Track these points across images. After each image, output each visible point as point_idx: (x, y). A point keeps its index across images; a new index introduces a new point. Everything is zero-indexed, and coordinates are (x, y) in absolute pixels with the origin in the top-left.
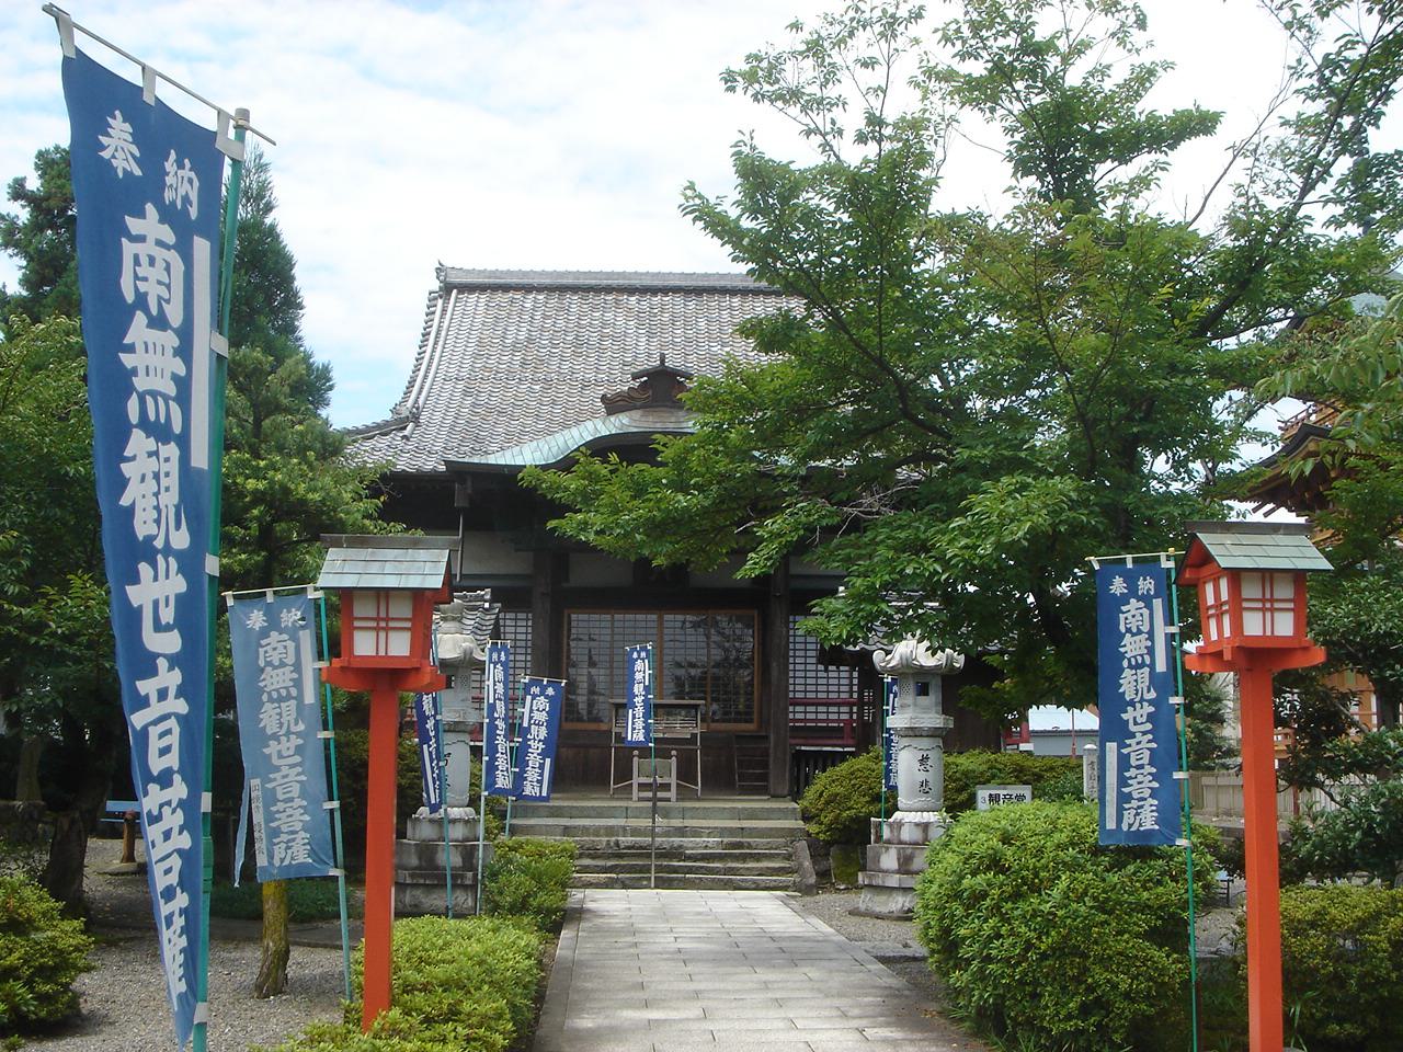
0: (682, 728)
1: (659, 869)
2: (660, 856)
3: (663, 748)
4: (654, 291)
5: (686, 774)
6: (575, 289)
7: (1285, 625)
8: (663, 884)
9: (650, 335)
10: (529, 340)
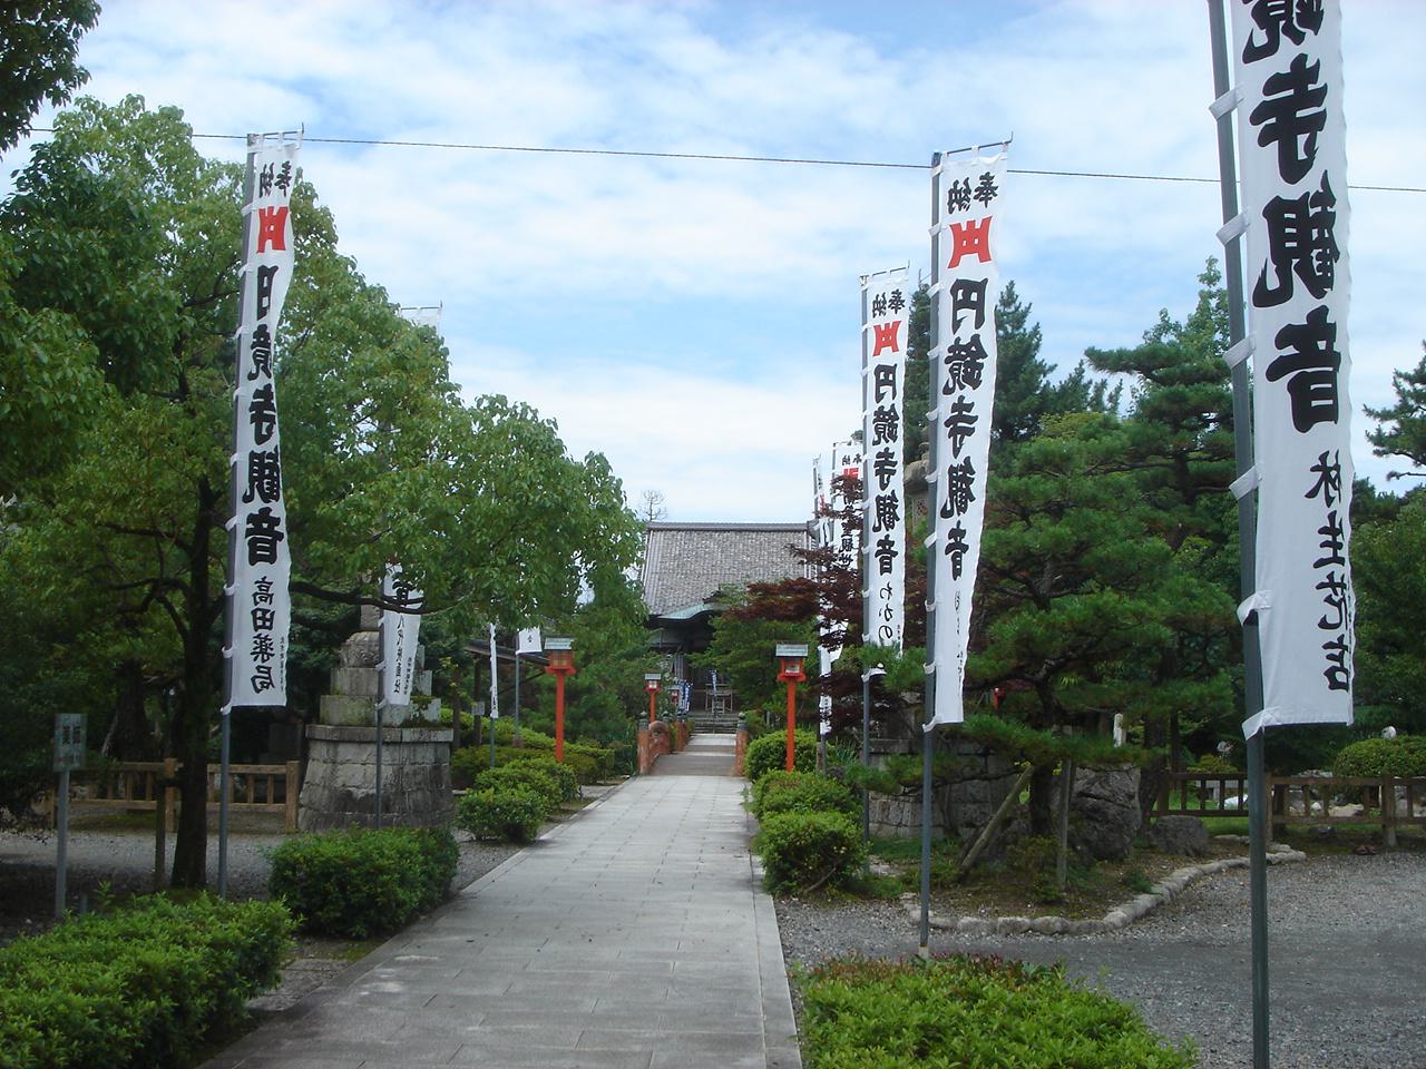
0: (727, 693)
3: (720, 699)
4: (725, 531)
5: (728, 705)
6: (791, 531)
7: (655, 687)
9: (722, 552)
10: (680, 555)
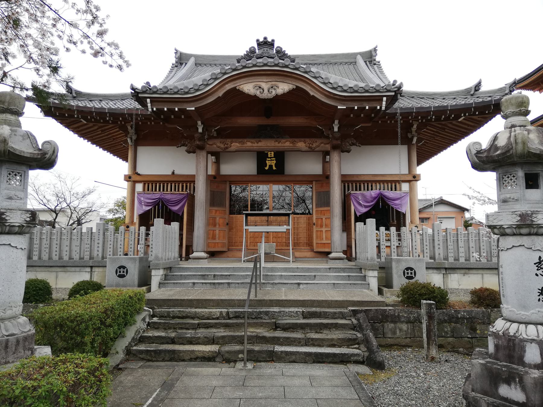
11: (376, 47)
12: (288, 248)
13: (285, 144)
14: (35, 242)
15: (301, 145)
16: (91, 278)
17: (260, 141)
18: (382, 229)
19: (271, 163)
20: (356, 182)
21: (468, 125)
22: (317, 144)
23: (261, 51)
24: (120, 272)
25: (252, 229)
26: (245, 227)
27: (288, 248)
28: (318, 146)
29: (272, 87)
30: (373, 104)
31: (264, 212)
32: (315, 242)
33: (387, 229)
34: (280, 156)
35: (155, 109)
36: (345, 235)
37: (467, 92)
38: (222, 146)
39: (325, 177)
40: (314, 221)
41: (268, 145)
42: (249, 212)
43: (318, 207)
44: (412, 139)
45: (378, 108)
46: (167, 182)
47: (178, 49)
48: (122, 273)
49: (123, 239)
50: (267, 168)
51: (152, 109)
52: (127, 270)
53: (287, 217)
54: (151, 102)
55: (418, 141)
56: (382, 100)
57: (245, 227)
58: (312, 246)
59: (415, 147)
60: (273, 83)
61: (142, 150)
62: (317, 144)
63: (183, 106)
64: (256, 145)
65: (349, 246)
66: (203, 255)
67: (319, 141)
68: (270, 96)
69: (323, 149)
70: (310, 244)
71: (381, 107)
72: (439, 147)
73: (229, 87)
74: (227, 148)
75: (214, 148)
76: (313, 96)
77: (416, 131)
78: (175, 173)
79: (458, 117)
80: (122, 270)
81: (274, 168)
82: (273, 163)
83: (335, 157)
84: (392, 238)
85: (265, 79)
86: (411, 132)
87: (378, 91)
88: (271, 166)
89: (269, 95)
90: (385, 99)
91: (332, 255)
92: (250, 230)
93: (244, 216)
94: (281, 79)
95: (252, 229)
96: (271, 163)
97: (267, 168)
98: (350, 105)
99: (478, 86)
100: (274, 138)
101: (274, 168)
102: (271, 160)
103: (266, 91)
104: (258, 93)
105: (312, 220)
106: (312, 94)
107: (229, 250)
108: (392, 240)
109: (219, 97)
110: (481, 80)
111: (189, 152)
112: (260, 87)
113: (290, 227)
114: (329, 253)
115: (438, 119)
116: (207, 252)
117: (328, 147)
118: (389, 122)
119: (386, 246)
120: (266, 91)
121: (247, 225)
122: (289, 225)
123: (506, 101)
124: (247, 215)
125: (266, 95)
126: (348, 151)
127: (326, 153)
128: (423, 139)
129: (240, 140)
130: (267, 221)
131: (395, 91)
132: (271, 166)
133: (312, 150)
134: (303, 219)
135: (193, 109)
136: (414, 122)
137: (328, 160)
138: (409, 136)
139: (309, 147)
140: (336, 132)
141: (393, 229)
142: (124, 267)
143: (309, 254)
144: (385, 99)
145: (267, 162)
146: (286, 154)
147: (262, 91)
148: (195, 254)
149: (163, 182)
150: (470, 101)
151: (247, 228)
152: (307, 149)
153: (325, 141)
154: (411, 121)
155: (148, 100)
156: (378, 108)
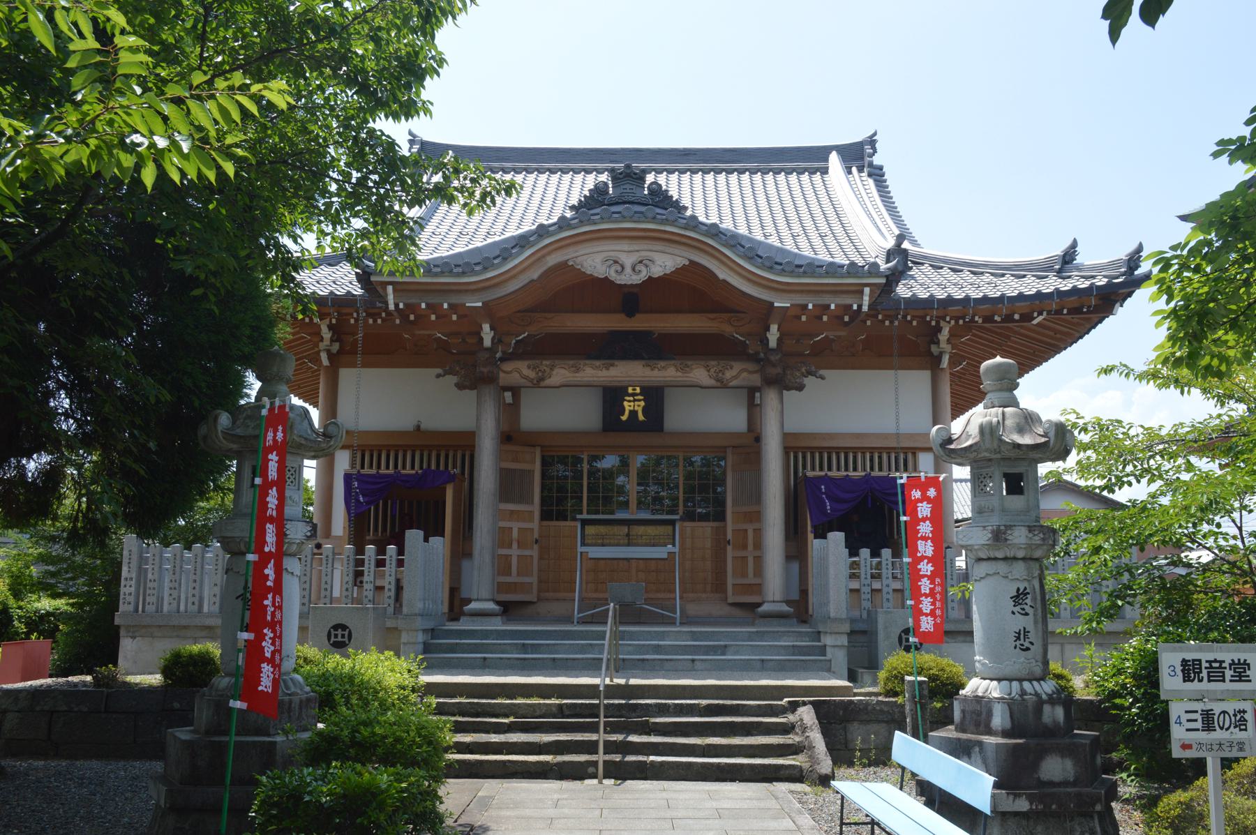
1: (611, 747)
2: (612, 728)
8: (620, 773)
11: (875, 134)
12: (672, 596)
13: (665, 373)
14: (150, 576)
15: (699, 374)
16: (956, 481)
17: (612, 365)
18: (865, 552)
19: (633, 406)
20: (821, 450)
21: (1056, 332)
22: (734, 372)
23: (619, 191)
24: (336, 636)
25: (595, 552)
26: (580, 549)
27: (672, 596)
28: (735, 377)
29: (641, 262)
30: (847, 300)
31: (620, 515)
32: (730, 581)
33: (875, 554)
34: (654, 396)
35: (401, 306)
36: (795, 566)
37: (1041, 269)
38: (532, 374)
39: (754, 437)
40: (729, 536)
41: (630, 373)
42: (585, 516)
43: (622, 623)
44: (939, 359)
45: (855, 307)
46: (405, 449)
47: (415, 131)
48: (339, 639)
49: (329, 570)
50: (624, 418)
51: (397, 305)
52: (329, 639)
53: (670, 528)
54: (395, 291)
55: (953, 363)
56: (862, 292)
57: (580, 549)
58: (725, 592)
59: (948, 376)
60: (644, 254)
61: (347, 375)
62: (734, 372)
63: (456, 299)
64: (605, 373)
65: (804, 593)
66: (491, 606)
67: (738, 366)
68: (637, 279)
69: (745, 383)
70: (719, 586)
71: (860, 307)
72: (1060, 340)
73: (553, 260)
74: (542, 379)
75: (515, 379)
76: (724, 281)
77: (949, 341)
78: (423, 427)
79: (1027, 317)
80: (340, 632)
81: (641, 417)
82: (639, 406)
83: (770, 399)
84: (884, 571)
85: (625, 246)
86: (938, 343)
87: (856, 275)
88: (633, 413)
89: (634, 277)
90: (867, 290)
91: (765, 608)
92: (591, 555)
93: (579, 525)
94: (659, 246)
95: (595, 552)
96: (633, 406)
97: (624, 418)
98: (800, 299)
99: (1068, 257)
100: (643, 358)
101: (641, 417)
102: (635, 400)
103: (628, 270)
104: (613, 276)
105: (725, 534)
106: (721, 276)
107: (539, 599)
108: (884, 576)
109: (532, 281)
110: (1075, 241)
111: (460, 386)
112: (616, 262)
113: (676, 550)
114: (759, 605)
115: (988, 319)
116: (498, 603)
117: (756, 380)
118: (887, 323)
119: (894, 590)
120: (628, 270)
121: (583, 544)
122: (674, 545)
123: (988, 369)
124: (585, 523)
125: (629, 278)
126: (800, 388)
127: (752, 391)
128: (964, 358)
129: (571, 362)
130: (628, 535)
131: (887, 277)
132: (633, 413)
133: (723, 385)
134: (707, 528)
135: (480, 304)
136: (942, 323)
137: (758, 401)
138: (934, 349)
139: (718, 380)
140: (772, 350)
141: (886, 553)
142: (344, 627)
143: (719, 609)
144: (867, 290)
145: (626, 404)
146: (667, 391)
147: (619, 269)
148: (473, 606)
149: (397, 448)
150: (1051, 284)
151: (585, 549)
152: (712, 382)
153: (751, 366)
154: (933, 323)
155: (390, 288)
156: (855, 307)
